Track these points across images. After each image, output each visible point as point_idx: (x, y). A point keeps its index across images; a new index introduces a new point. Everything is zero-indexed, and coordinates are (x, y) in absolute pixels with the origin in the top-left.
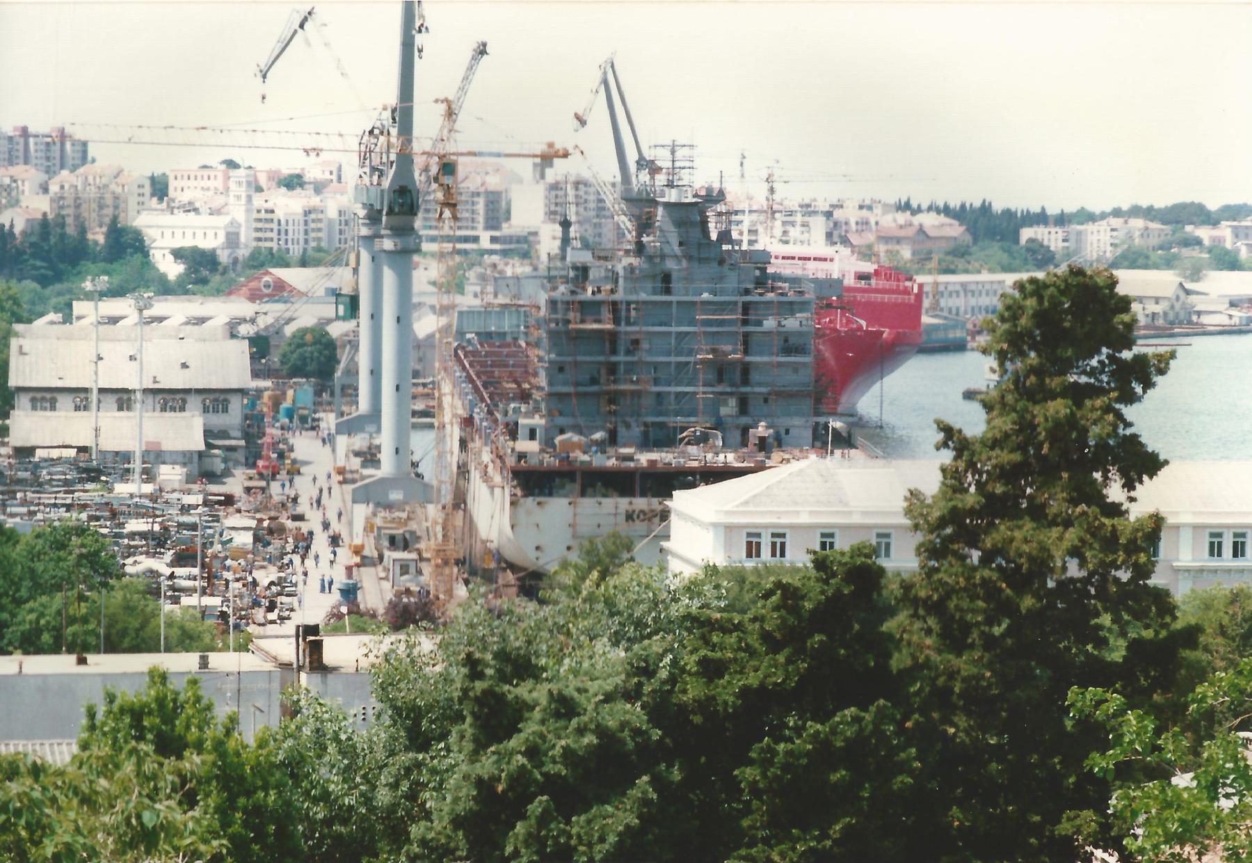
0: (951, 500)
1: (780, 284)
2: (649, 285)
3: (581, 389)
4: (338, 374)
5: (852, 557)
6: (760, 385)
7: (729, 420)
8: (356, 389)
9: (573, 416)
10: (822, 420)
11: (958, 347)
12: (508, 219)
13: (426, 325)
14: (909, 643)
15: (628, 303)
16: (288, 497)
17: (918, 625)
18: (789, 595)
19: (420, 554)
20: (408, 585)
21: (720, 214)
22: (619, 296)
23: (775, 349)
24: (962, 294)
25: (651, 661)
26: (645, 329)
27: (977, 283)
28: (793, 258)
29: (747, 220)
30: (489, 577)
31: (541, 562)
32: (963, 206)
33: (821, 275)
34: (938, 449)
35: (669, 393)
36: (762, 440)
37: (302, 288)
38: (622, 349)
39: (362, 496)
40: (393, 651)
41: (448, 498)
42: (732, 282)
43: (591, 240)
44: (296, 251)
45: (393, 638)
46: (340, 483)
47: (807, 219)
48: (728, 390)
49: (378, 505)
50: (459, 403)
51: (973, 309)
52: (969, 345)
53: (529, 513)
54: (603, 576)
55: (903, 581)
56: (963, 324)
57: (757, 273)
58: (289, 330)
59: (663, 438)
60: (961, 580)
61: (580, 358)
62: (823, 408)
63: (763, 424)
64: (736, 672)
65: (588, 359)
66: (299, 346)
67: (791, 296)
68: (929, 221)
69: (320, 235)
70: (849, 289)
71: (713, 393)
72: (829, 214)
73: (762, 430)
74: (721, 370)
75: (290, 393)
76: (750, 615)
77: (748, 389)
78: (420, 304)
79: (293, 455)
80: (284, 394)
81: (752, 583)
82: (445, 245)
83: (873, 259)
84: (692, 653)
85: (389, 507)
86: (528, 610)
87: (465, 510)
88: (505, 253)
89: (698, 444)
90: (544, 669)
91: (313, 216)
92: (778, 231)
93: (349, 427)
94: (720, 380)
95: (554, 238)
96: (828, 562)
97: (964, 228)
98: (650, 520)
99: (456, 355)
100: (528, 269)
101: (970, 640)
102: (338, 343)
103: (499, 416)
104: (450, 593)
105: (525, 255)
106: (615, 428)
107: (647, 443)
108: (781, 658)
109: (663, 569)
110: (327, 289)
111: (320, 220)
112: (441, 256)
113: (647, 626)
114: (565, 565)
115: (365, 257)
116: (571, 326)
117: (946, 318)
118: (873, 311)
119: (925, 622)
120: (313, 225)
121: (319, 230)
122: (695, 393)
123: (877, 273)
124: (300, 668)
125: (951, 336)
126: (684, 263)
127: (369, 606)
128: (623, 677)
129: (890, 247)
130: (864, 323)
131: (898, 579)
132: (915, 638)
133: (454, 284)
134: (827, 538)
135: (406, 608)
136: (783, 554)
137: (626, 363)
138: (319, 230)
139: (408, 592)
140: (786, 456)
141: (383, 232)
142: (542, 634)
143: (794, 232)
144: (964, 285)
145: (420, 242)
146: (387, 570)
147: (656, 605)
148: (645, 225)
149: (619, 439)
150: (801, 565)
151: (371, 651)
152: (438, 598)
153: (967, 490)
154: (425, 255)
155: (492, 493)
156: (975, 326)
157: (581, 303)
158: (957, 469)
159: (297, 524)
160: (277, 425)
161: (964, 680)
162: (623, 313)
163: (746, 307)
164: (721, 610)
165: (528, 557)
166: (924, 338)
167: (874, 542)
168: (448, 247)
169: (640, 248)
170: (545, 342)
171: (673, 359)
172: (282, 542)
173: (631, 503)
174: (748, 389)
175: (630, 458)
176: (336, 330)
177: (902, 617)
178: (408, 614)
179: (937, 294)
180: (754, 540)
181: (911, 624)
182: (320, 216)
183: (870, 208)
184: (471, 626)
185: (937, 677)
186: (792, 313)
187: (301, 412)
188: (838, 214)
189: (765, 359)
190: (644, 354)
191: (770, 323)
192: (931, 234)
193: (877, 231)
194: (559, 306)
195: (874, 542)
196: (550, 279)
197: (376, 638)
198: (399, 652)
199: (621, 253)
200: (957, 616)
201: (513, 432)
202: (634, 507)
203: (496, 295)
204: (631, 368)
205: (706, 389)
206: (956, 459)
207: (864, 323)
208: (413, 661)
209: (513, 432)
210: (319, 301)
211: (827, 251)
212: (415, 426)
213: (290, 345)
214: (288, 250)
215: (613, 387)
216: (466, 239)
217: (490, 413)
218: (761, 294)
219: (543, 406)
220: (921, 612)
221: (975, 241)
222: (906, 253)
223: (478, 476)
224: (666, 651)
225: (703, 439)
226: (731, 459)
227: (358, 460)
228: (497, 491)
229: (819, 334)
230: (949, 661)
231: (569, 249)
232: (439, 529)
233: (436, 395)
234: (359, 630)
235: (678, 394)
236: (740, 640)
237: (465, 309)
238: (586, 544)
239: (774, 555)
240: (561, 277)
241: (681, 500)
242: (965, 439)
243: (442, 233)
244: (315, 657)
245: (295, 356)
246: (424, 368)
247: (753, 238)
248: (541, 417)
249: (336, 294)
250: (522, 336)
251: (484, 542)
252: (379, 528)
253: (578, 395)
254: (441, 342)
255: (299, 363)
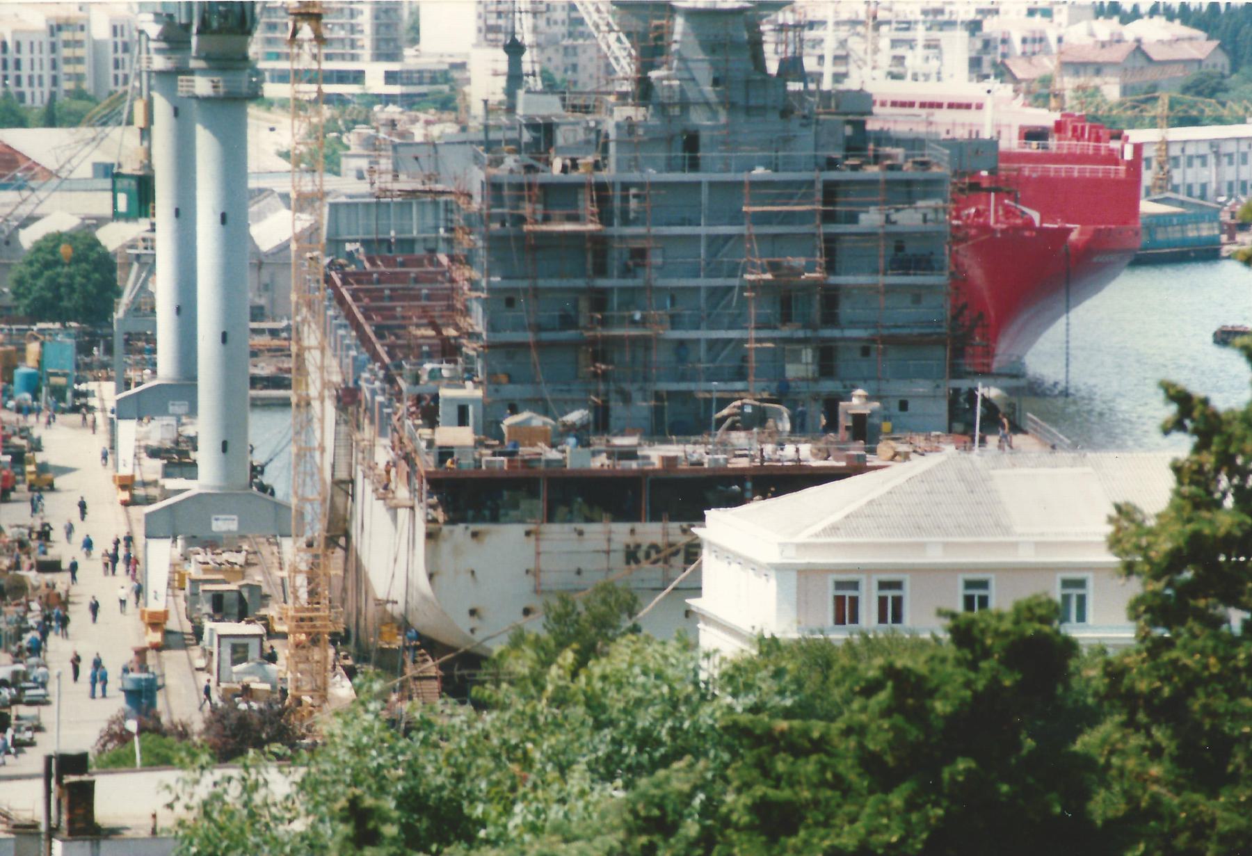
0: (1190, 520)
1: (888, 150)
2: (661, 155)
3: (545, 336)
4: (119, 314)
5: (1017, 622)
6: (853, 324)
7: (803, 387)
8: (152, 340)
9: (532, 381)
10: (964, 384)
11: (1208, 253)
12: (415, 41)
13: (273, 228)
14: (1122, 772)
15: (626, 186)
16: (31, 530)
17: (1136, 740)
18: (908, 689)
19: (267, 626)
20: (247, 679)
21: (782, 28)
22: (606, 175)
23: (881, 263)
24: (1212, 160)
25: (670, 808)
26: (655, 230)
27: (1238, 139)
28: (912, 104)
29: (830, 39)
30: (388, 663)
31: (478, 637)
32: (1214, 7)
33: (961, 133)
34: (1166, 431)
35: (698, 341)
36: (859, 420)
37: (50, 163)
38: (614, 264)
39: (166, 525)
40: (216, 797)
41: (317, 529)
42: (804, 148)
43: (558, 76)
44: (36, 97)
45: (218, 774)
46: (125, 504)
47: (935, 34)
48: (800, 334)
49: (192, 540)
50: (333, 364)
51: (1231, 185)
52: (1225, 250)
53: (457, 551)
54: (582, 662)
55: (1108, 663)
56: (1214, 215)
57: (849, 130)
58: (28, 238)
59: (689, 419)
60: (1212, 661)
61: (542, 283)
62: (967, 364)
63: (860, 392)
64: (817, 824)
65: (555, 283)
66: (47, 265)
67: (909, 171)
68: (1153, 32)
69: (80, 69)
70: (1009, 157)
71: (773, 340)
72: (974, 27)
73: (857, 402)
74: (786, 300)
75: (33, 348)
76: (839, 724)
77: (836, 333)
78: (261, 191)
79: (40, 457)
80: (22, 350)
81: (843, 668)
82: (304, 87)
83: (1053, 103)
84: (739, 791)
85: (212, 543)
86: (457, 721)
87: (347, 549)
88: (409, 101)
89: (747, 428)
90: (482, 823)
91: (65, 35)
92: (884, 59)
93: (137, 407)
94: (786, 318)
95: (496, 74)
96: (976, 632)
97: (1215, 43)
98: (666, 561)
99: (328, 280)
100: (450, 129)
101: (1230, 768)
102: (118, 261)
103: (403, 384)
104: (322, 693)
105: (446, 104)
106: (606, 402)
107: (658, 431)
108: (896, 800)
109: (689, 645)
110: (96, 166)
111: (79, 43)
112: (298, 107)
113: (659, 743)
114: (518, 640)
115: (162, 107)
116: (527, 227)
117: (1182, 204)
118: (1050, 193)
119: (1149, 735)
120: (67, 52)
121: (79, 60)
122: (743, 341)
123: (1059, 127)
124: (52, 832)
125: (1192, 234)
126: (723, 117)
127: (176, 719)
128: (621, 834)
129: (1082, 80)
130: (1036, 216)
131: (1099, 660)
132: (1131, 764)
133: (323, 156)
134: (976, 590)
135: (243, 721)
136: (897, 618)
137: (622, 290)
138: (79, 60)
139: (247, 692)
140: (903, 448)
141: (193, 64)
142: (480, 761)
143: (914, 59)
144: (1214, 144)
145: (263, 81)
146: (208, 654)
147: (675, 706)
148: (651, 50)
149: (612, 422)
150: (926, 636)
151: (178, 798)
152: (299, 702)
153: (1218, 504)
154: (269, 104)
155: (395, 518)
156: (1233, 216)
157: (545, 187)
158: (1201, 466)
159: (49, 577)
160: (11, 404)
161: (1223, 839)
162: (617, 203)
163: (831, 192)
164: (788, 714)
165: (456, 628)
166: (1144, 239)
167: (1057, 596)
168: (308, 90)
169: (644, 91)
170: (482, 256)
171: (703, 282)
172: (21, 609)
173: (632, 531)
174: (836, 333)
175: (630, 454)
176: (113, 237)
177: (1109, 728)
178: (244, 732)
179: (1168, 161)
180: (848, 593)
181: (1124, 738)
182: (79, 36)
183: (1047, 13)
184: (358, 750)
185: (1174, 834)
186: (910, 199)
187: (53, 380)
188: (991, 26)
189: (863, 279)
190: (654, 274)
191: (871, 219)
192: (1156, 56)
193: (1061, 53)
194: (506, 192)
195: (1057, 596)
196: (489, 145)
197: (188, 775)
198: (228, 799)
199: (612, 99)
200: (1207, 724)
201: (429, 413)
202: (638, 539)
203: (396, 177)
204: (632, 297)
205: (764, 334)
206: (1197, 449)
207: (1036, 216)
208: (252, 815)
209: (429, 413)
210: (82, 186)
211: (973, 90)
212: (257, 404)
213: (30, 263)
214: (21, 96)
215: (600, 332)
216: (342, 77)
217: (390, 379)
218: (854, 168)
219: (479, 365)
220: (1141, 717)
221: (1235, 68)
222: (1111, 90)
223: (369, 489)
224: (695, 789)
225: (756, 421)
226: (805, 452)
227: (158, 464)
228: (403, 514)
229: (958, 236)
230: (1194, 805)
231: (521, 94)
232: (301, 580)
233: (294, 349)
234: (159, 761)
235: (712, 343)
236: (823, 767)
237: (343, 199)
238: (555, 603)
239: (882, 619)
240: (508, 142)
241: (719, 526)
242: (1216, 415)
243: (296, 66)
244: (79, 812)
245: (41, 283)
246: (273, 302)
247: (842, 69)
248: (477, 384)
249: (110, 173)
250: (442, 245)
251: (379, 603)
252: (195, 582)
253: (540, 345)
254: (299, 255)
255: (49, 295)
